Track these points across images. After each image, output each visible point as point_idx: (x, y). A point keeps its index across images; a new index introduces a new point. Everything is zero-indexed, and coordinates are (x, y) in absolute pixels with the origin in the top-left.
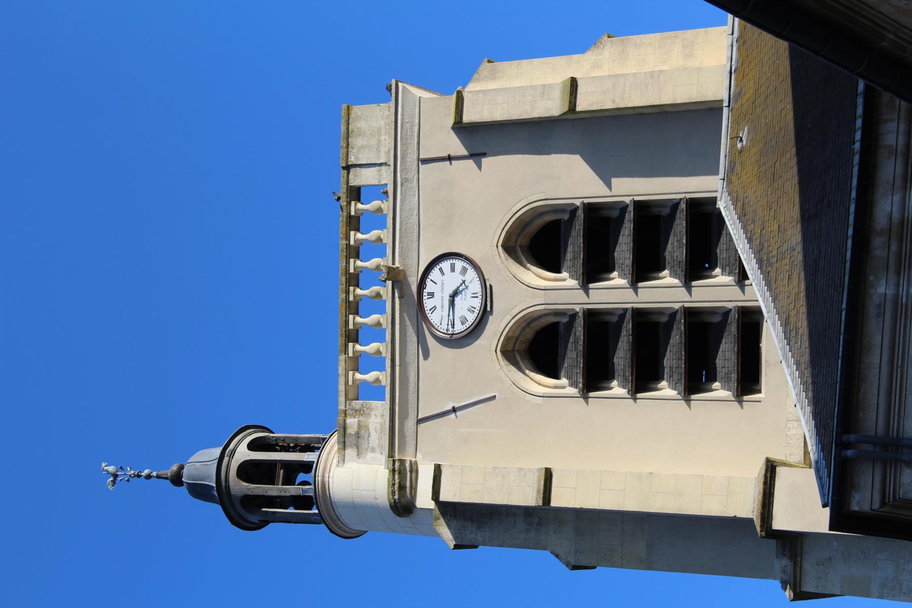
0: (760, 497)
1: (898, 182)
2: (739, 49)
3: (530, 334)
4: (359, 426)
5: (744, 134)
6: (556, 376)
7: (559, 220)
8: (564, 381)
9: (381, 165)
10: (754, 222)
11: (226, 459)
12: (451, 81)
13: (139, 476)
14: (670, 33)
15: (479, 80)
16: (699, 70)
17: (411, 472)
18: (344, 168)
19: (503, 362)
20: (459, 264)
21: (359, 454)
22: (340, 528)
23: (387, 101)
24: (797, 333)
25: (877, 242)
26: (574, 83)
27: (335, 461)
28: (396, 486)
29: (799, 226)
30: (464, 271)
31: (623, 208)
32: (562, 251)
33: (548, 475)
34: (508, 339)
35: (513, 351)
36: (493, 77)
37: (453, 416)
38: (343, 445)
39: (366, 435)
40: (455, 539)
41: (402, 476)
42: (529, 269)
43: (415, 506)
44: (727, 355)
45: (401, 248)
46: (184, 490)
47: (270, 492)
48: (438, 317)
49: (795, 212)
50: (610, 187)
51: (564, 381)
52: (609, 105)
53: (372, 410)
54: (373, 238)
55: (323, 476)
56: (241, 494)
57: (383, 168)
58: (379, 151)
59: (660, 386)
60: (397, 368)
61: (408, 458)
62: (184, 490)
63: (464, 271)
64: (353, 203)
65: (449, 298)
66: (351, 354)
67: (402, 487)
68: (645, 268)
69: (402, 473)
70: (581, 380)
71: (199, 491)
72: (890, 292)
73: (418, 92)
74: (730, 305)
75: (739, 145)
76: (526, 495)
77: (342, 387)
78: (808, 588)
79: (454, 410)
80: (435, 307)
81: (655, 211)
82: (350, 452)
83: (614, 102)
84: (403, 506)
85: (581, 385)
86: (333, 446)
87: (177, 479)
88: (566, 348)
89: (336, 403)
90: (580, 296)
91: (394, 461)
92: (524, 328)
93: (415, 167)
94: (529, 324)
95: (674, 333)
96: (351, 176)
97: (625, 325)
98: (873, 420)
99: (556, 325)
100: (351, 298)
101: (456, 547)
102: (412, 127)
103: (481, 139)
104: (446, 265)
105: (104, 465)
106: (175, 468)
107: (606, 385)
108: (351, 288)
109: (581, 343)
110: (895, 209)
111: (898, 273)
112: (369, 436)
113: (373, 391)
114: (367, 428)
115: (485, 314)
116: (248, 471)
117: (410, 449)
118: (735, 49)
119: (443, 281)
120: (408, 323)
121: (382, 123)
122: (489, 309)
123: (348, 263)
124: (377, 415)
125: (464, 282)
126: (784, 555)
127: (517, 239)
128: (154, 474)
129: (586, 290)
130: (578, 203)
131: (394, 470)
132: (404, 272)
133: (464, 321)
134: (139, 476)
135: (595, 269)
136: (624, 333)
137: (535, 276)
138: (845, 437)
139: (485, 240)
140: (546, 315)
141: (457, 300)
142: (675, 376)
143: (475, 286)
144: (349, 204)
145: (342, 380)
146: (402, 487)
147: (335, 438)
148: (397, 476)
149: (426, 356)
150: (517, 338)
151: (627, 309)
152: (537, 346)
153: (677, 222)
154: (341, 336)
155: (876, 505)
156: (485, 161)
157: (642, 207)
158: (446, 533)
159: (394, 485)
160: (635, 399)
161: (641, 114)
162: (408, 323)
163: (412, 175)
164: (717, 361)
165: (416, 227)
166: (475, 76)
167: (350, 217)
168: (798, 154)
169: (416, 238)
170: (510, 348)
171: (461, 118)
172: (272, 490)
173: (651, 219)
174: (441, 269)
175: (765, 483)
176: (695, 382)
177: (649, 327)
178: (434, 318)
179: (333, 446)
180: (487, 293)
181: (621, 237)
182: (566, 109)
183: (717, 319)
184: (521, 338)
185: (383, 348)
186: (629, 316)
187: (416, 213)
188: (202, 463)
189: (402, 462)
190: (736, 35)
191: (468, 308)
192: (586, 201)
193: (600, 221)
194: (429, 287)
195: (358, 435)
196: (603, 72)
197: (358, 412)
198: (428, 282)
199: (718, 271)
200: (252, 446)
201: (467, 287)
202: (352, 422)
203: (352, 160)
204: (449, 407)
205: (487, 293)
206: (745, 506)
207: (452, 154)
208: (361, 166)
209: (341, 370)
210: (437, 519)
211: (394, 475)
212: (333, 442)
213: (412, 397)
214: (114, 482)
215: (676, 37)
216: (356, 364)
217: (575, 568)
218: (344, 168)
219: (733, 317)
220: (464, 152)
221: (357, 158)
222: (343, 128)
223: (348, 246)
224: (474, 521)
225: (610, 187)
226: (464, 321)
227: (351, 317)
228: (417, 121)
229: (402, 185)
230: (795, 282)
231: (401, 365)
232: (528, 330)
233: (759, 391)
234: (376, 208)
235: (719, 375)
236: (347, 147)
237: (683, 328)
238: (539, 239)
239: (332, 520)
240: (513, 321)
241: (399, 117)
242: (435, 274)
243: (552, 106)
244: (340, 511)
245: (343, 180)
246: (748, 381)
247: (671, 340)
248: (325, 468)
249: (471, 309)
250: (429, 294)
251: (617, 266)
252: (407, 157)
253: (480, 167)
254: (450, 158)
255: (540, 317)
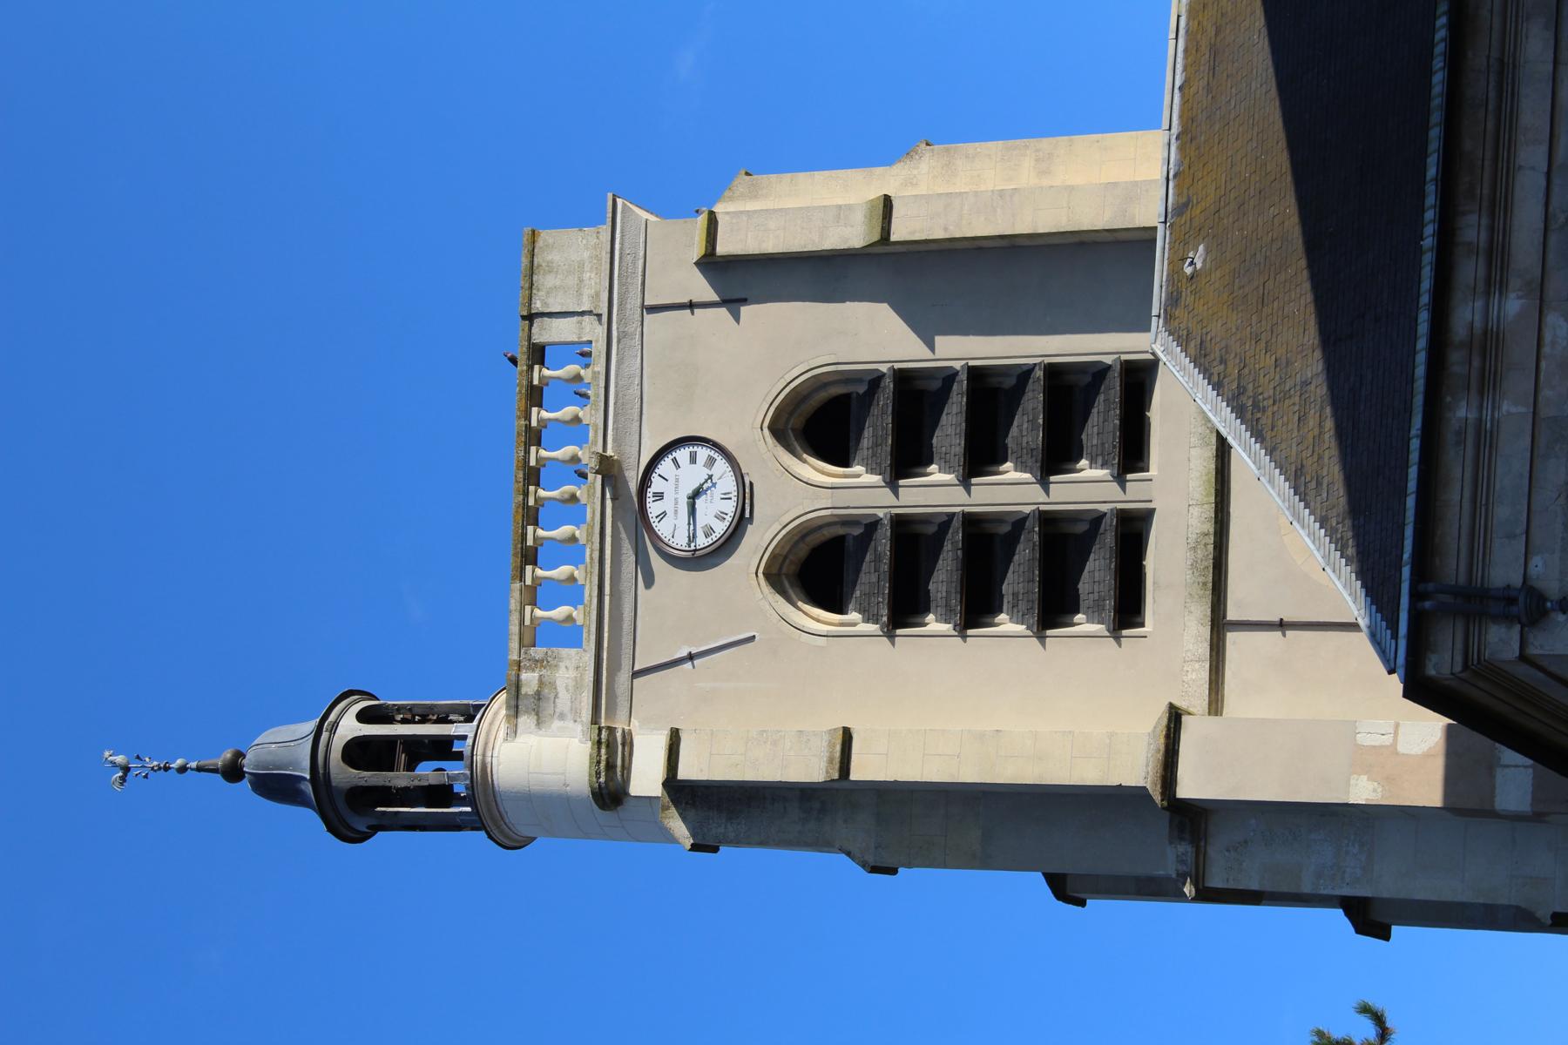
0: (1160, 756)
1: (1481, 286)
2: (1181, 149)
3: (803, 551)
4: (541, 682)
5: (1199, 256)
6: (840, 610)
7: (848, 396)
8: (854, 616)
9: (583, 313)
10: (1223, 361)
11: (325, 735)
12: (693, 198)
13: (166, 769)
14: (1018, 142)
15: (731, 199)
16: (1070, 189)
17: (623, 745)
18: (523, 318)
19: (767, 589)
20: (703, 453)
21: (539, 724)
22: (502, 832)
23: (594, 222)
24: (1319, 484)
25: (1455, 358)
26: (887, 202)
27: (502, 734)
28: (603, 765)
29: (1318, 354)
30: (711, 462)
31: (949, 377)
32: (853, 436)
33: (847, 736)
34: (773, 557)
35: (779, 574)
36: (753, 195)
37: (688, 665)
38: (515, 710)
39: (552, 696)
40: (693, 835)
41: (612, 753)
42: (805, 461)
43: (626, 794)
44: (1097, 575)
45: (614, 440)
46: (245, 784)
47: (392, 784)
48: (671, 526)
49: (1312, 336)
50: (932, 349)
51: (854, 616)
52: (939, 234)
53: (561, 660)
54: (568, 417)
55: (484, 755)
56: (348, 786)
57: (586, 318)
58: (579, 294)
59: (997, 620)
60: (607, 599)
61: (620, 726)
62: (245, 784)
63: (711, 462)
64: (537, 367)
65: (685, 502)
66: (529, 582)
67: (610, 767)
68: (981, 457)
69: (611, 746)
70: (885, 612)
71: (276, 787)
72: (1472, 416)
73: (644, 215)
74: (1104, 508)
75: (1188, 270)
76: (812, 768)
77: (514, 628)
78: (1216, 881)
79: (691, 657)
80: (664, 514)
81: (994, 381)
82: (526, 721)
83: (946, 229)
84: (610, 793)
85: (885, 619)
86: (496, 714)
87: (233, 772)
88: (858, 571)
89: (506, 650)
90: (885, 497)
91: (600, 729)
92: (796, 544)
93: (637, 316)
94: (803, 537)
95: (1020, 547)
96: (535, 330)
97: (949, 536)
98: (1452, 567)
99: (839, 541)
100: (531, 502)
101: (694, 848)
102: (634, 263)
103: (739, 279)
104: (682, 454)
105: (107, 754)
106: (228, 755)
107: (919, 620)
108: (532, 488)
109: (886, 560)
110: (1477, 318)
111: (1481, 393)
112: (556, 696)
113: (567, 634)
114: (553, 685)
115: (742, 521)
116: (358, 751)
117: (622, 713)
118: (1173, 149)
119: (676, 478)
120: (623, 535)
121: (586, 255)
122: (747, 515)
123: (527, 452)
124: (571, 671)
125: (710, 477)
126: (1181, 839)
127: (788, 420)
128: (193, 765)
129: (894, 488)
130: (884, 368)
131: (599, 742)
132: (619, 463)
133: (709, 532)
134: (166, 769)
135: (907, 459)
136: (948, 546)
137: (814, 470)
138: (1421, 587)
139: (744, 421)
140: (829, 525)
141: (699, 502)
142: (1022, 606)
143: (728, 483)
144: (531, 368)
145: (515, 618)
146: (610, 767)
147: (503, 697)
148: (603, 751)
149: (649, 583)
150: (786, 557)
151: (954, 514)
152: (818, 569)
153: (1029, 395)
154: (515, 555)
155: (1458, 668)
156: (745, 310)
157: (977, 375)
158: (678, 826)
159: (599, 762)
160: (964, 637)
161: (980, 249)
162: (623, 535)
163: (634, 327)
164: (1080, 586)
165: (637, 400)
166: (726, 193)
167: (531, 387)
168: (1310, 266)
169: (636, 417)
170: (774, 570)
171: (714, 248)
172: (399, 778)
173: (991, 394)
174: (675, 460)
175: (1167, 736)
176: (1053, 611)
177: (986, 541)
178: (663, 529)
179: (496, 714)
180: (746, 493)
181: (944, 416)
182: (876, 237)
183: (1081, 528)
184: (791, 557)
185: (584, 575)
186: (957, 523)
187: (637, 381)
188: (284, 743)
189: (611, 730)
190: (1175, 130)
191: (716, 513)
192: (897, 366)
193: (916, 395)
194: (656, 484)
195: (538, 696)
196: (922, 190)
197: (538, 663)
198: (655, 478)
199: (1084, 463)
200: (364, 717)
201: (714, 485)
202: (530, 679)
203: (538, 306)
204: (684, 653)
205: (746, 493)
206: (1133, 768)
207: (695, 300)
208: (542, 315)
209: (514, 604)
210: (665, 808)
211: (599, 749)
212: (499, 707)
213: (626, 640)
214: (123, 779)
215: (1027, 147)
216: (532, 596)
217: (875, 869)
218: (523, 318)
219: (1109, 526)
220: (715, 298)
221: (545, 304)
222: (525, 261)
223: (528, 427)
224: (723, 811)
225: (932, 349)
226: (709, 532)
227: (530, 529)
228: (642, 253)
229: (619, 342)
230: (1312, 422)
231: (611, 595)
232: (801, 545)
233: (1142, 625)
234: (573, 374)
235: (1083, 605)
236: (531, 288)
237: (1036, 538)
238: (822, 420)
239: (493, 818)
240: (784, 532)
241: (617, 246)
242: (665, 466)
243: (854, 234)
244: (507, 807)
245: (522, 335)
246: (1127, 610)
247: (1016, 558)
248: (486, 744)
249: (720, 517)
250: (655, 495)
251: (936, 458)
252: (626, 306)
253: (737, 319)
254: (691, 306)
255: (820, 527)
